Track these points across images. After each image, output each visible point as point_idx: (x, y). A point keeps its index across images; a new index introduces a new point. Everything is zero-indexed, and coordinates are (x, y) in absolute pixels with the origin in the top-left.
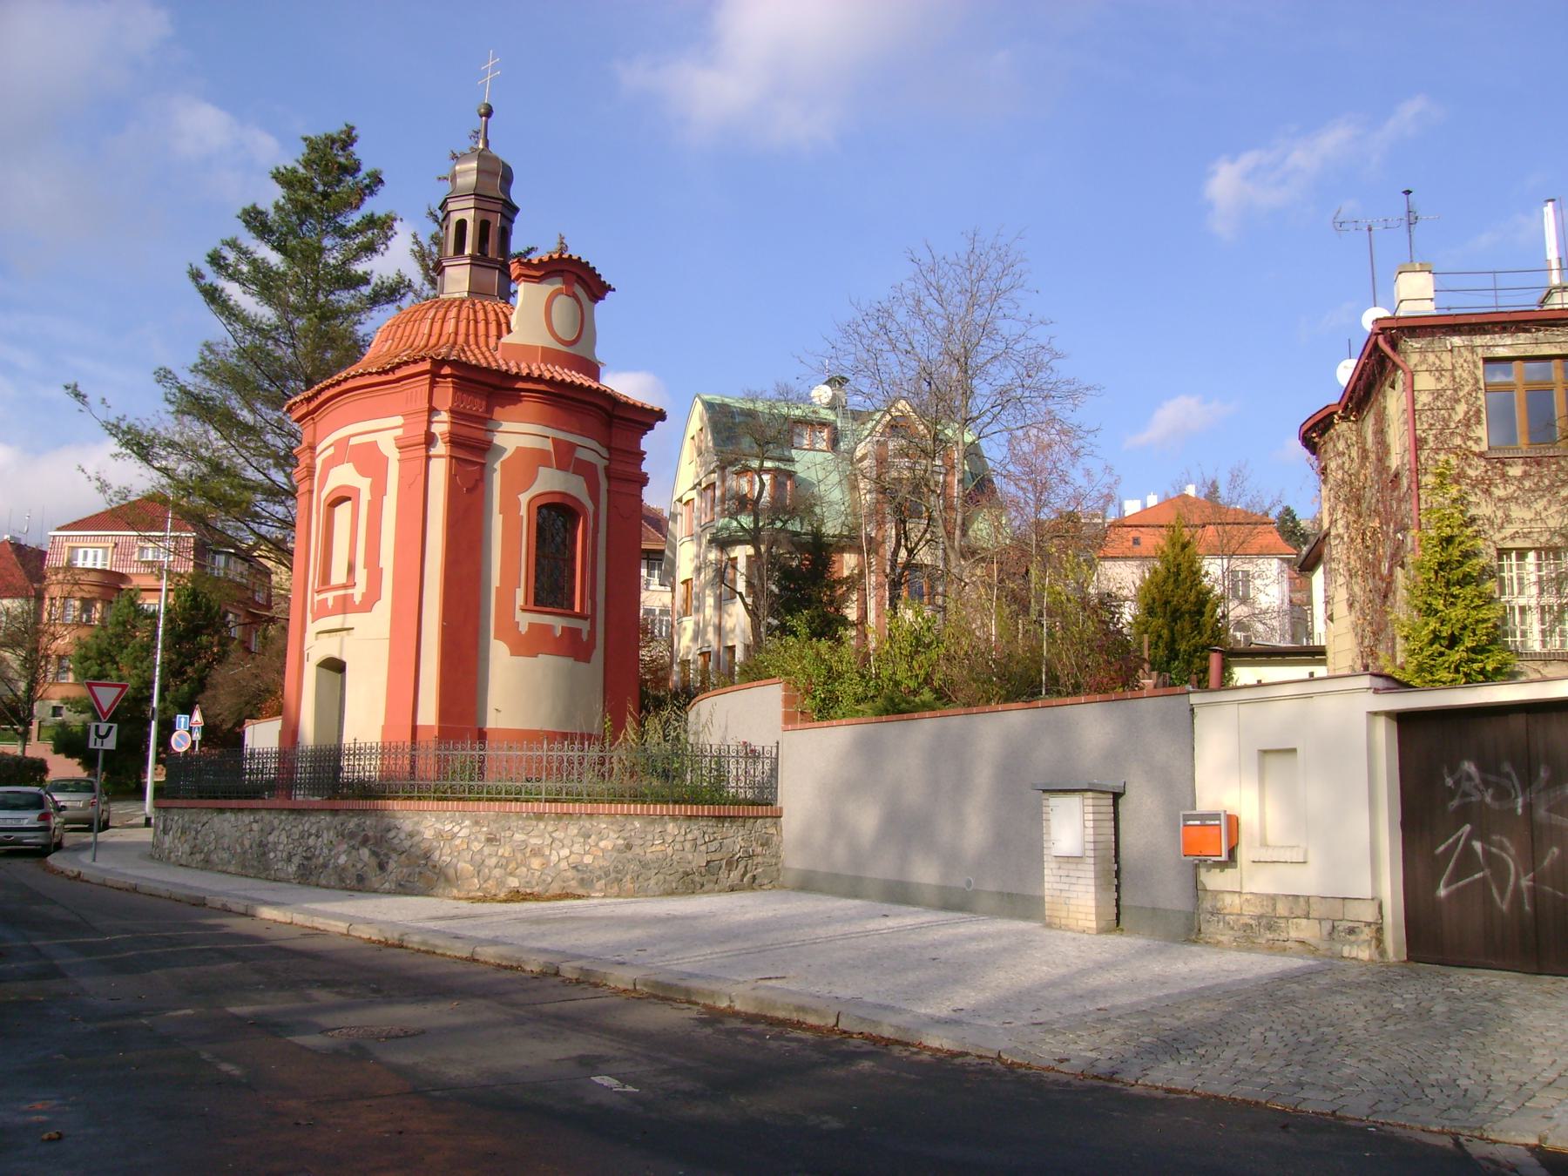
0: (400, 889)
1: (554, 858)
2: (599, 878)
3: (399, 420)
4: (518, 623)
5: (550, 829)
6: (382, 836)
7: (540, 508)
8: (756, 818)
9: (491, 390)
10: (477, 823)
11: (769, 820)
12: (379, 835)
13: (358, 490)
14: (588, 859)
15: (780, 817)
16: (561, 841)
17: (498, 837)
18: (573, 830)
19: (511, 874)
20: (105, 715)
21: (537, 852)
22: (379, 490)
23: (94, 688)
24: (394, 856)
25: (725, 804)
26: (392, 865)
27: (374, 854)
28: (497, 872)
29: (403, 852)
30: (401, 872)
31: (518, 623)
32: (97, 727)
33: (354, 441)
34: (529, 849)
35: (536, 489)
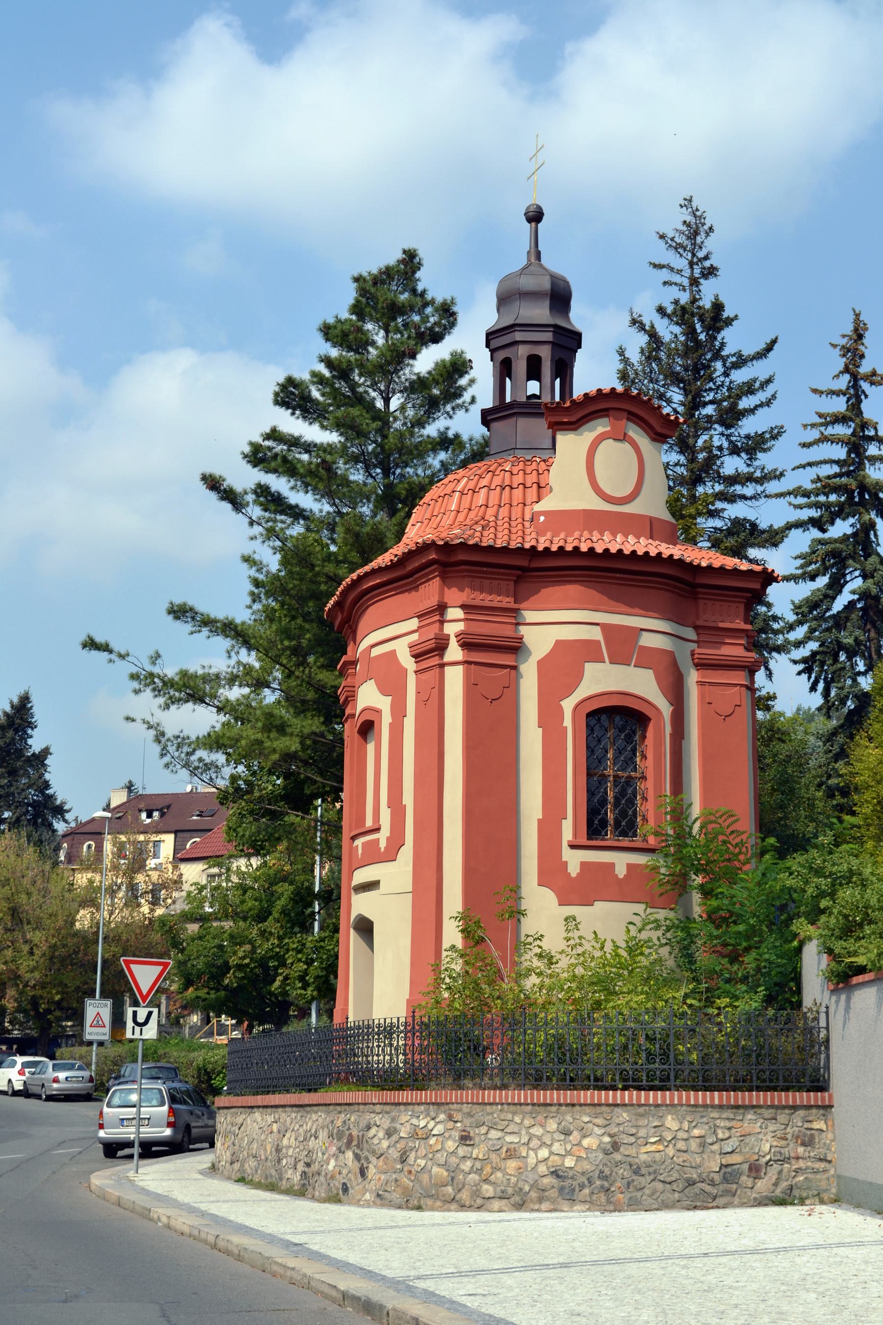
0: (378, 1201)
1: (532, 1160)
2: (582, 1186)
3: (414, 623)
4: (566, 863)
5: (527, 1122)
6: (363, 1135)
7: (589, 715)
8: (795, 1108)
9: (519, 572)
10: (450, 1118)
11: (814, 1111)
12: (360, 1134)
13: (378, 712)
14: (569, 1162)
15: (832, 1106)
16: (539, 1138)
17: (472, 1134)
18: (552, 1125)
19: (486, 1181)
20: (144, 998)
21: (511, 1154)
22: (399, 712)
23: (132, 966)
24: (373, 1159)
25: (485, 1089)
26: (372, 1171)
27: (357, 1157)
28: (473, 1177)
29: (382, 1155)
30: (380, 1179)
31: (566, 863)
32: (135, 1013)
33: (375, 652)
34: (504, 1149)
35: (583, 691)
